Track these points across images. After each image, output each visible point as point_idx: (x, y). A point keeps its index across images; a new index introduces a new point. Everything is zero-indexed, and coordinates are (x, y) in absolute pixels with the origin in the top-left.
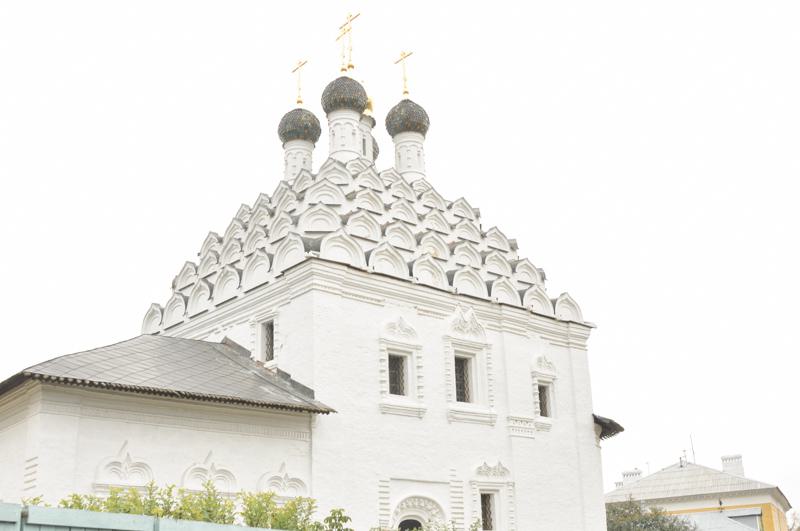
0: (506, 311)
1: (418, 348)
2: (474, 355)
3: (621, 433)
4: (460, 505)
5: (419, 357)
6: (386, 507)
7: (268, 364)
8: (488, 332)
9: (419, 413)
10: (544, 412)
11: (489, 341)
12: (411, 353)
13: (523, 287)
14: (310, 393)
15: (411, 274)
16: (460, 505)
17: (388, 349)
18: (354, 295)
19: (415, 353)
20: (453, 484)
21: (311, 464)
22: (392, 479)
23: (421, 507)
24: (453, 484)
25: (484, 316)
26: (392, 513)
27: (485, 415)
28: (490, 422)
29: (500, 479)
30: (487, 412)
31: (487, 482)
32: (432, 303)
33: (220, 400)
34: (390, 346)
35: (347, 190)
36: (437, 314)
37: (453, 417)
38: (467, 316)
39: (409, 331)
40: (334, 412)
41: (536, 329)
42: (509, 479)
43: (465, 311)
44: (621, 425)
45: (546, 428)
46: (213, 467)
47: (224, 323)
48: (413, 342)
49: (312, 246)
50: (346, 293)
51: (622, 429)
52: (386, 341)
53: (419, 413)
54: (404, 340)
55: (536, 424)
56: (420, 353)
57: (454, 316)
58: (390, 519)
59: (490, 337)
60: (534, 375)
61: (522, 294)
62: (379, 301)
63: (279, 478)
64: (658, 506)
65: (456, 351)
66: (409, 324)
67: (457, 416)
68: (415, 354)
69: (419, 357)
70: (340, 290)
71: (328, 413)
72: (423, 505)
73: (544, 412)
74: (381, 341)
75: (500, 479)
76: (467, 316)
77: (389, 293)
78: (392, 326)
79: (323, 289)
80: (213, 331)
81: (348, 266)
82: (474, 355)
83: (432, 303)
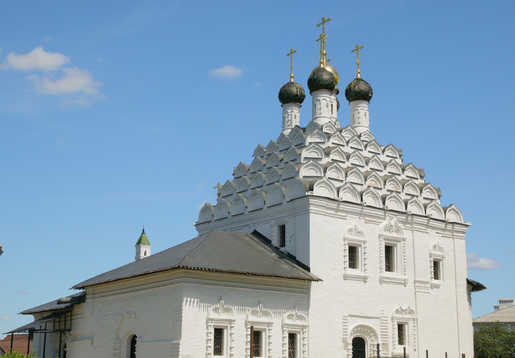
0: (416, 219)
1: (364, 242)
8: (404, 231)
9: (365, 279)
10: (436, 276)
11: (405, 237)
13: (428, 202)
15: (362, 200)
20: (382, 318)
22: (500, 302)
24: (382, 318)
25: (405, 223)
26: (349, 333)
27: (401, 280)
28: (405, 284)
29: (409, 316)
30: (403, 277)
31: (401, 317)
37: (382, 281)
38: (393, 222)
39: (360, 233)
41: (434, 228)
43: (391, 219)
44: (485, 286)
45: (437, 287)
47: (254, 222)
48: (362, 239)
52: (348, 239)
53: (365, 279)
54: (357, 238)
55: (431, 284)
57: (385, 223)
59: (407, 234)
60: (431, 255)
62: (344, 216)
66: (360, 228)
67: (385, 280)
68: (363, 246)
71: (318, 281)
73: (436, 276)
75: (409, 316)
76: (393, 222)
79: (315, 212)
80: (247, 225)
81: (328, 198)
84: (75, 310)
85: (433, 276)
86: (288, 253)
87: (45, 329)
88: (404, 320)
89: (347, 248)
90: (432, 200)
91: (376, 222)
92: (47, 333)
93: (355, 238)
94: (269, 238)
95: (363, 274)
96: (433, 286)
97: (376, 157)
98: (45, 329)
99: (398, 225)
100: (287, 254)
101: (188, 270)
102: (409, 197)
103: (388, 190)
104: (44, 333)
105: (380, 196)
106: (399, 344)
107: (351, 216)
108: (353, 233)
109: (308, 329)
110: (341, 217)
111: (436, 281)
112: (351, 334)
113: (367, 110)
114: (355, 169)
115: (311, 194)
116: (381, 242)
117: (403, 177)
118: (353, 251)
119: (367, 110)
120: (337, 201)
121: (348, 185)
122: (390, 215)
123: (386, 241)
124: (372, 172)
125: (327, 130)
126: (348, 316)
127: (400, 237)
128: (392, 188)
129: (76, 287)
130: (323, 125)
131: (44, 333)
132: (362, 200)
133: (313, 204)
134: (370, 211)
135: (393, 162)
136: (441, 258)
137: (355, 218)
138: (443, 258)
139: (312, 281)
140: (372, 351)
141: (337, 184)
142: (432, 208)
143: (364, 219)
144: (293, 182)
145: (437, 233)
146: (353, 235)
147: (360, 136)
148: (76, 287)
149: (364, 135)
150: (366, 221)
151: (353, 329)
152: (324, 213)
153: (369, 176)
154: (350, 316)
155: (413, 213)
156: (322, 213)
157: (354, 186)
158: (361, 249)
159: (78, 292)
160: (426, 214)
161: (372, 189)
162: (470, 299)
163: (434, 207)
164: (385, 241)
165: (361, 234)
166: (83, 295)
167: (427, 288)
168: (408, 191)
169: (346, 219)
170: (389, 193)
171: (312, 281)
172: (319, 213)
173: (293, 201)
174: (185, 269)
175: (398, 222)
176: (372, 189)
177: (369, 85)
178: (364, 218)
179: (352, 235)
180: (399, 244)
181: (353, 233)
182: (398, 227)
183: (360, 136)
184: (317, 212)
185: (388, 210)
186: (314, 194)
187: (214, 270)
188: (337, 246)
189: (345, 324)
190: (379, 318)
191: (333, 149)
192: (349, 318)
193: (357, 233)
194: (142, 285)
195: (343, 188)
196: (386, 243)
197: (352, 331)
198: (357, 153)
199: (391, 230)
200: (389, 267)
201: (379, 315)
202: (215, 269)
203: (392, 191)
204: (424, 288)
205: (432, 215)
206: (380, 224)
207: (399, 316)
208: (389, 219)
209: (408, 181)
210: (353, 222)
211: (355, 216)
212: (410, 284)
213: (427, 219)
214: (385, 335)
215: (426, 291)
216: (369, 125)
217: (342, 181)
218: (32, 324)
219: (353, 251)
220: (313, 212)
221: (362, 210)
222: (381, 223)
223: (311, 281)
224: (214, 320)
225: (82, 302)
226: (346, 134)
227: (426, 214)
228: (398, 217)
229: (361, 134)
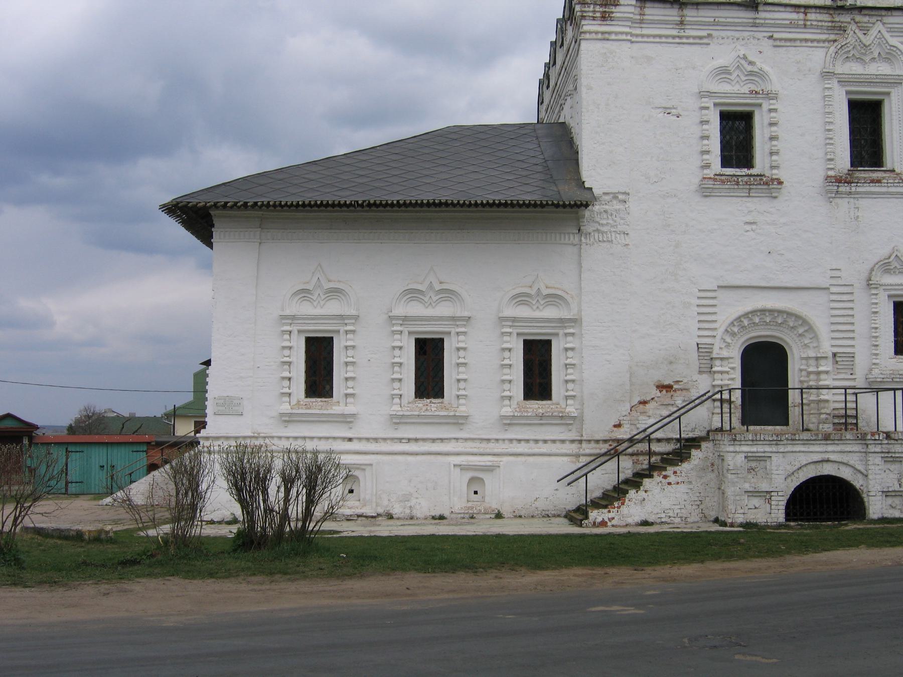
2: (888, 94)
3: (209, 249)
4: (850, 320)
5: (770, 110)
12: (760, 105)
16: (850, 320)
17: (715, 105)
18: (655, 36)
20: (833, 289)
21: (580, 272)
22: (718, 287)
23: (767, 324)
24: (833, 289)
33: (333, 205)
34: (718, 101)
36: (790, 40)
46: (431, 286)
50: (637, 36)
51: (212, 248)
52: (710, 94)
56: (774, 104)
62: (701, 38)
63: (528, 295)
64: (632, 444)
65: (848, 93)
68: (766, 106)
69: (770, 110)
70: (627, 34)
72: (768, 320)
74: (702, 94)
78: (723, 72)
82: (888, 94)
87: (896, 391)
88: (895, 290)
92: (858, 395)
98: (896, 391)
99: (887, 42)
104: (800, 390)
107: (723, 34)
108: (732, 77)
109: (705, 322)
116: (826, 91)
126: (716, 289)
131: (800, 390)
137: (738, 39)
140: (804, 373)
143: (771, 37)
146: (733, 83)
152: (629, 37)
156: (624, 37)
158: (762, 116)
165: (759, 77)
175: (887, 35)
178: (771, 34)
179: (730, 83)
181: (732, 77)
182: (888, 47)
192: (722, 294)
193: (747, 75)
194: (709, 313)
199: (867, 59)
201: (824, 282)
211: (737, 34)
224: (459, 320)
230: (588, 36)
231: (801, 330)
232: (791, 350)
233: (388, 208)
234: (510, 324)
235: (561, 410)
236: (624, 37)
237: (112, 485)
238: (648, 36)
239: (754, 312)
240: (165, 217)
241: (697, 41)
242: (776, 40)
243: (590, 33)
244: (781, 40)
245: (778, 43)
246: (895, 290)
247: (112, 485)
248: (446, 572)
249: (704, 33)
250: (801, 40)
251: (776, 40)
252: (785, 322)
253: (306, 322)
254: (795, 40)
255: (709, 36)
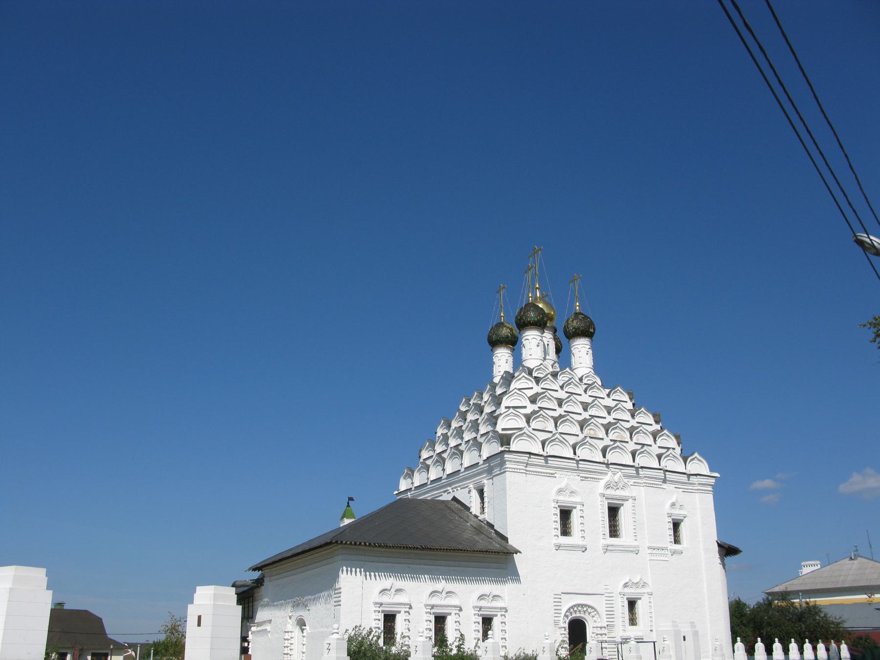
6: (559, 611)
7: (481, 517)
10: (677, 541)
14: (505, 539)
15: (575, 453)
17: (559, 506)
19: (579, 507)
20: (606, 595)
22: (562, 593)
26: (562, 615)
31: (632, 592)
32: (590, 472)
35: (530, 393)
37: (607, 549)
40: (520, 552)
42: (649, 590)
49: (505, 440)
57: (607, 478)
58: (561, 619)
60: (670, 515)
61: (659, 457)
62: (552, 474)
70: (524, 470)
73: (677, 541)
77: (559, 468)
79: (513, 470)
83: (590, 472)
84: (256, 595)
85: (673, 540)
86: (488, 522)
89: (558, 512)
90: (521, 429)
91: (595, 478)
93: (566, 500)
94: (467, 505)
95: (580, 542)
96: (674, 553)
97: (596, 402)
100: (485, 523)
101: (351, 546)
102: (664, 451)
103: (611, 440)
105: (571, 444)
106: (630, 625)
107: (561, 472)
109: (557, 610)
110: (548, 475)
111: (677, 545)
112: (566, 616)
113: (589, 348)
114: (568, 417)
115: (507, 449)
117: (633, 423)
118: (565, 514)
119: (589, 348)
120: (541, 456)
121: (557, 436)
122: (612, 470)
123: (609, 501)
124: (590, 419)
125: (538, 374)
127: (628, 495)
128: (617, 437)
129: (255, 569)
130: (534, 368)
132: (575, 453)
133: (508, 461)
134: (594, 467)
135: (619, 406)
136: (683, 518)
138: (685, 517)
139: (515, 555)
141: (543, 436)
142: (669, 458)
143: (579, 476)
144: (489, 437)
145: (676, 488)
147: (581, 379)
148: (255, 569)
149: (586, 377)
150: (582, 478)
151: (568, 609)
152: (525, 471)
153: (533, 417)
154: (562, 593)
155: (642, 466)
157: (563, 436)
159: (257, 575)
160: (660, 465)
161: (588, 439)
162: (724, 565)
163: (671, 457)
164: (607, 501)
166: (261, 577)
167: (665, 555)
168: (638, 439)
169: (556, 477)
170: (612, 443)
171: (515, 555)
172: (518, 471)
173: (489, 459)
174: (362, 546)
176: (588, 439)
177: (590, 319)
180: (626, 503)
183: (581, 379)
184: (516, 470)
185: (609, 463)
186: (511, 450)
187: (376, 544)
188: (544, 510)
189: (558, 603)
190: (603, 595)
191: (541, 395)
192: (563, 596)
195: (550, 440)
196: (608, 503)
197: (567, 612)
198: (572, 397)
200: (614, 531)
202: (378, 544)
203: (615, 441)
204: (660, 555)
205: (666, 467)
206: (600, 480)
207: (627, 590)
208: (612, 475)
209: (637, 428)
210: (564, 479)
212: (645, 553)
213: (662, 471)
214: (610, 614)
215: (664, 559)
216: (593, 366)
217: (551, 432)
218: (244, 608)
219: (565, 514)
220: (511, 470)
221: (578, 466)
222: (601, 479)
223: (513, 553)
225: (260, 586)
226: (588, 380)
227: (660, 465)
228: (622, 471)
229: (582, 376)
230: (508, 470)
231: (593, 614)
232: (587, 622)
233: (475, 552)
234: (500, 610)
235: (372, 635)
236: (523, 471)
237: (54, 632)
238: (532, 471)
239: (575, 606)
240: (742, 550)
241: (551, 475)
242: (581, 477)
243: (510, 468)
244: (583, 477)
245: (582, 478)
246: (629, 595)
247: (54, 632)
248: (5, 623)
249: (553, 472)
250: (591, 478)
251: (581, 477)
252: (587, 610)
253: (386, 606)
254: (588, 478)
255: (556, 473)
